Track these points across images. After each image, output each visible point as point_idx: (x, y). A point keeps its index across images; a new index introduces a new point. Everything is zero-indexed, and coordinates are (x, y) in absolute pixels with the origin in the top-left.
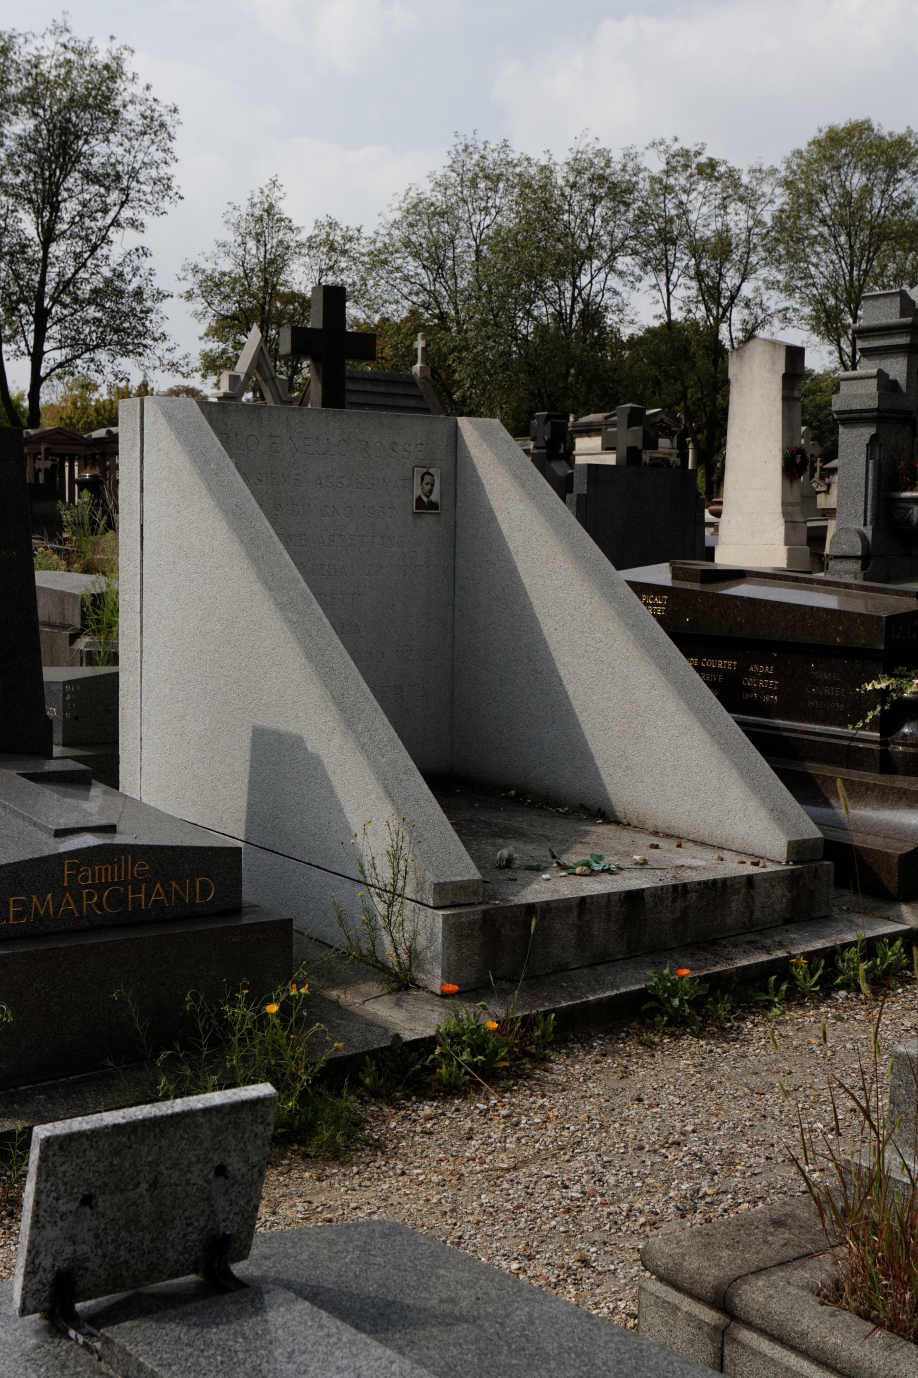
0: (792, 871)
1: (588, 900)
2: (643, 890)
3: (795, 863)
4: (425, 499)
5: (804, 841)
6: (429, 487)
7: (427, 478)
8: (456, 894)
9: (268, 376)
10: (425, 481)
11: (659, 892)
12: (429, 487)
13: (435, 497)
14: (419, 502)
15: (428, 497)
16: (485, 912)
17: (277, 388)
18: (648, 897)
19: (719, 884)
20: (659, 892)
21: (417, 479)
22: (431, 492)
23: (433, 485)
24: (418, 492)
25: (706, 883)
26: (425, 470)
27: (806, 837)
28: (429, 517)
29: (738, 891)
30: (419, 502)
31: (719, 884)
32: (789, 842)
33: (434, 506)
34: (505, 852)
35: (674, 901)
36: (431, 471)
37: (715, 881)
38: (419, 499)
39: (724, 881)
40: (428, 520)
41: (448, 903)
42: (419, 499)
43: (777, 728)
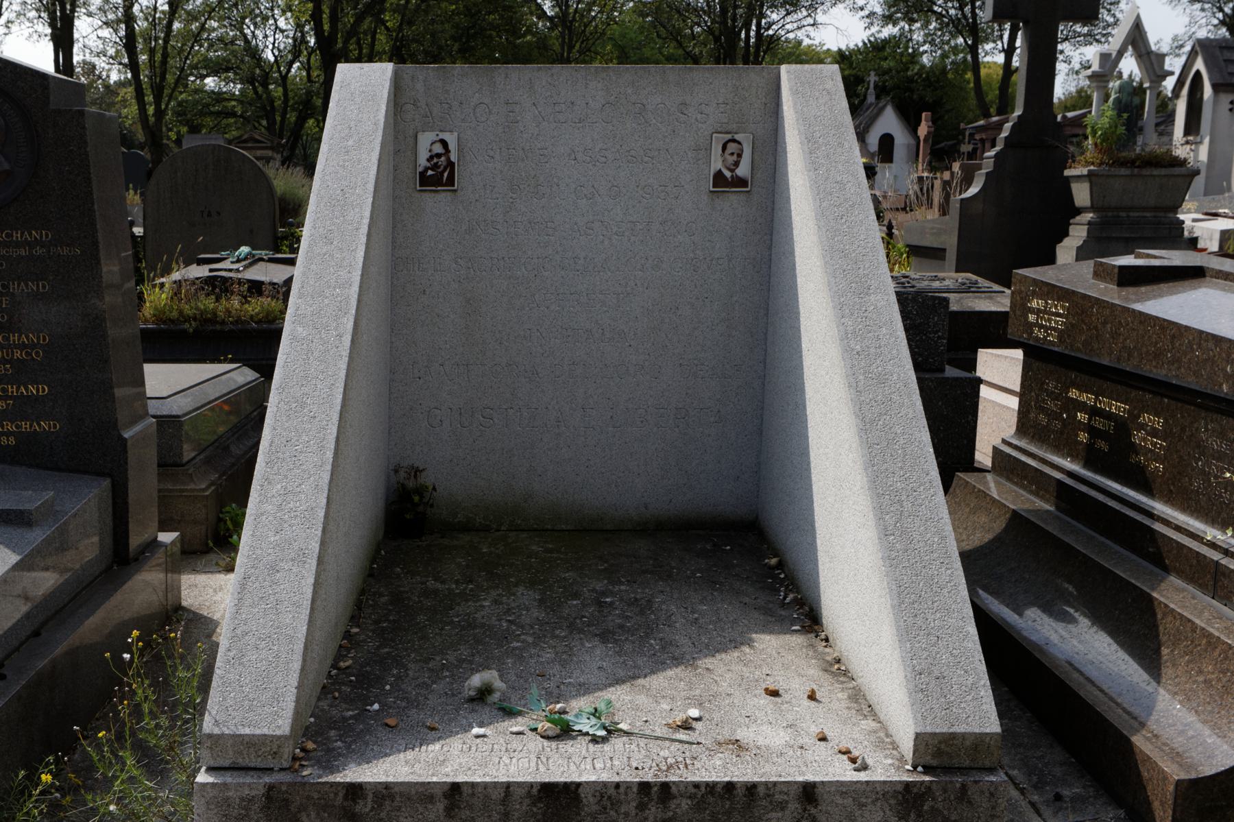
0: (907, 785)
1: (464, 789)
2: (579, 785)
3: (928, 770)
4: (728, 174)
5: (953, 736)
6: (735, 158)
7: (732, 147)
8: (241, 753)
9: (1144, 52)
10: (728, 151)
11: (612, 791)
12: (735, 158)
13: (743, 170)
14: (719, 178)
15: (732, 171)
16: (271, 788)
17: (1152, 64)
18: (588, 798)
19: (740, 792)
20: (612, 791)
21: (717, 149)
22: (737, 164)
23: (740, 156)
24: (717, 164)
25: (711, 787)
26: (729, 136)
27: (960, 729)
28: (733, 197)
29: (782, 806)
30: (719, 178)
31: (740, 792)
32: (918, 736)
33: (742, 182)
34: (476, 680)
35: (642, 807)
36: (737, 137)
37: (730, 786)
38: (719, 176)
39: (751, 788)
40: (733, 201)
41: (227, 763)
42: (719, 176)
43: (1150, 514)
